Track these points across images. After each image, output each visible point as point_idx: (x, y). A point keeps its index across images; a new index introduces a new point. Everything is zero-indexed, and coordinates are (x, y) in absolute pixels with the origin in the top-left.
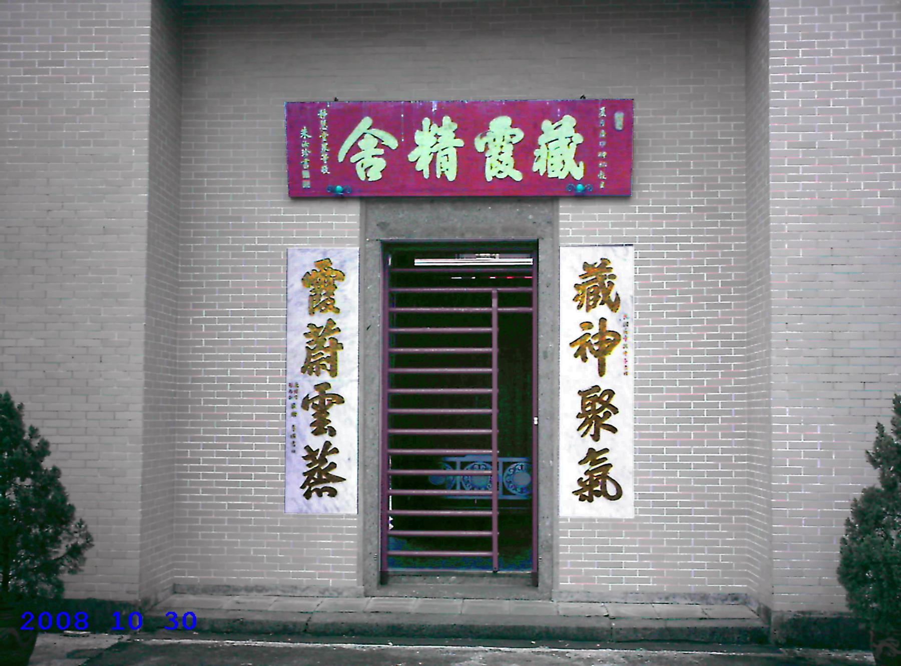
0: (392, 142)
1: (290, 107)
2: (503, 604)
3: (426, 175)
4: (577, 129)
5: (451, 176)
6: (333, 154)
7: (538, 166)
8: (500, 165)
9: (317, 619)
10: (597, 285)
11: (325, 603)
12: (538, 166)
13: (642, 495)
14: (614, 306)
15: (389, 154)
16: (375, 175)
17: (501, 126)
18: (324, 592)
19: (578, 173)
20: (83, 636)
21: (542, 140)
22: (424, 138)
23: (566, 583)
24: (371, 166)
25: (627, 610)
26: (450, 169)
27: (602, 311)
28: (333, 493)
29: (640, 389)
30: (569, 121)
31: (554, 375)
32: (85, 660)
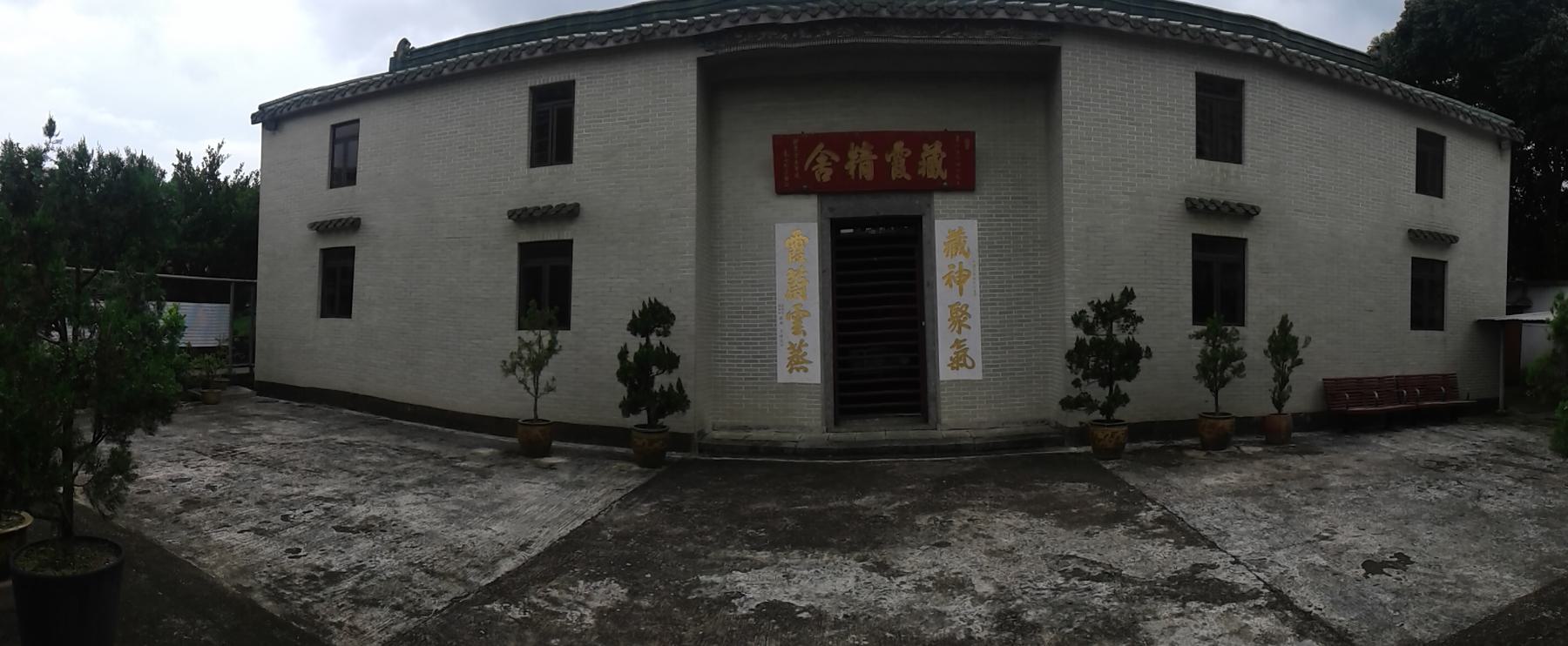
0: (836, 158)
1: (775, 137)
2: (912, 433)
3: (852, 173)
4: (943, 149)
5: (168, 178)
6: (802, 166)
7: (921, 172)
8: (898, 172)
9: (801, 446)
10: (957, 245)
11: (804, 436)
12: (921, 172)
13: (986, 366)
14: (967, 254)
15: (834, 165)
16: (826, 178)
17: (898, 146)
18: (802, 428)
19: (944, 176)
20: (723, 428)
21: (923, 156)
22: (852, 155)
23: (945, 419)
24: (824, 173)
25: (982, 433)
26: (868, 173)
27: (961, 258)
28: (806, 370)
29: (983, 304)
30: (938, 146)
31: (934, 296)
32: (620, 495)
